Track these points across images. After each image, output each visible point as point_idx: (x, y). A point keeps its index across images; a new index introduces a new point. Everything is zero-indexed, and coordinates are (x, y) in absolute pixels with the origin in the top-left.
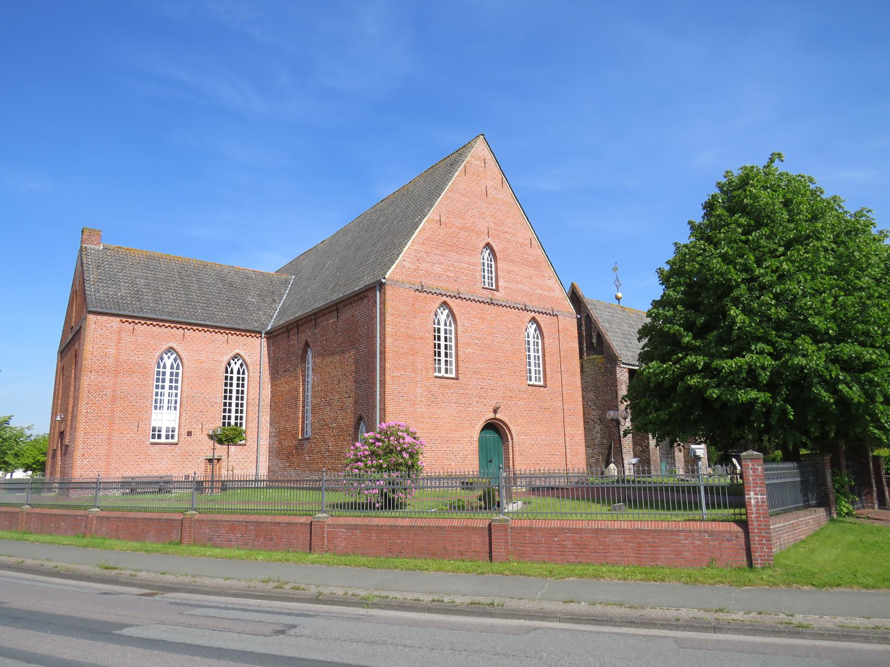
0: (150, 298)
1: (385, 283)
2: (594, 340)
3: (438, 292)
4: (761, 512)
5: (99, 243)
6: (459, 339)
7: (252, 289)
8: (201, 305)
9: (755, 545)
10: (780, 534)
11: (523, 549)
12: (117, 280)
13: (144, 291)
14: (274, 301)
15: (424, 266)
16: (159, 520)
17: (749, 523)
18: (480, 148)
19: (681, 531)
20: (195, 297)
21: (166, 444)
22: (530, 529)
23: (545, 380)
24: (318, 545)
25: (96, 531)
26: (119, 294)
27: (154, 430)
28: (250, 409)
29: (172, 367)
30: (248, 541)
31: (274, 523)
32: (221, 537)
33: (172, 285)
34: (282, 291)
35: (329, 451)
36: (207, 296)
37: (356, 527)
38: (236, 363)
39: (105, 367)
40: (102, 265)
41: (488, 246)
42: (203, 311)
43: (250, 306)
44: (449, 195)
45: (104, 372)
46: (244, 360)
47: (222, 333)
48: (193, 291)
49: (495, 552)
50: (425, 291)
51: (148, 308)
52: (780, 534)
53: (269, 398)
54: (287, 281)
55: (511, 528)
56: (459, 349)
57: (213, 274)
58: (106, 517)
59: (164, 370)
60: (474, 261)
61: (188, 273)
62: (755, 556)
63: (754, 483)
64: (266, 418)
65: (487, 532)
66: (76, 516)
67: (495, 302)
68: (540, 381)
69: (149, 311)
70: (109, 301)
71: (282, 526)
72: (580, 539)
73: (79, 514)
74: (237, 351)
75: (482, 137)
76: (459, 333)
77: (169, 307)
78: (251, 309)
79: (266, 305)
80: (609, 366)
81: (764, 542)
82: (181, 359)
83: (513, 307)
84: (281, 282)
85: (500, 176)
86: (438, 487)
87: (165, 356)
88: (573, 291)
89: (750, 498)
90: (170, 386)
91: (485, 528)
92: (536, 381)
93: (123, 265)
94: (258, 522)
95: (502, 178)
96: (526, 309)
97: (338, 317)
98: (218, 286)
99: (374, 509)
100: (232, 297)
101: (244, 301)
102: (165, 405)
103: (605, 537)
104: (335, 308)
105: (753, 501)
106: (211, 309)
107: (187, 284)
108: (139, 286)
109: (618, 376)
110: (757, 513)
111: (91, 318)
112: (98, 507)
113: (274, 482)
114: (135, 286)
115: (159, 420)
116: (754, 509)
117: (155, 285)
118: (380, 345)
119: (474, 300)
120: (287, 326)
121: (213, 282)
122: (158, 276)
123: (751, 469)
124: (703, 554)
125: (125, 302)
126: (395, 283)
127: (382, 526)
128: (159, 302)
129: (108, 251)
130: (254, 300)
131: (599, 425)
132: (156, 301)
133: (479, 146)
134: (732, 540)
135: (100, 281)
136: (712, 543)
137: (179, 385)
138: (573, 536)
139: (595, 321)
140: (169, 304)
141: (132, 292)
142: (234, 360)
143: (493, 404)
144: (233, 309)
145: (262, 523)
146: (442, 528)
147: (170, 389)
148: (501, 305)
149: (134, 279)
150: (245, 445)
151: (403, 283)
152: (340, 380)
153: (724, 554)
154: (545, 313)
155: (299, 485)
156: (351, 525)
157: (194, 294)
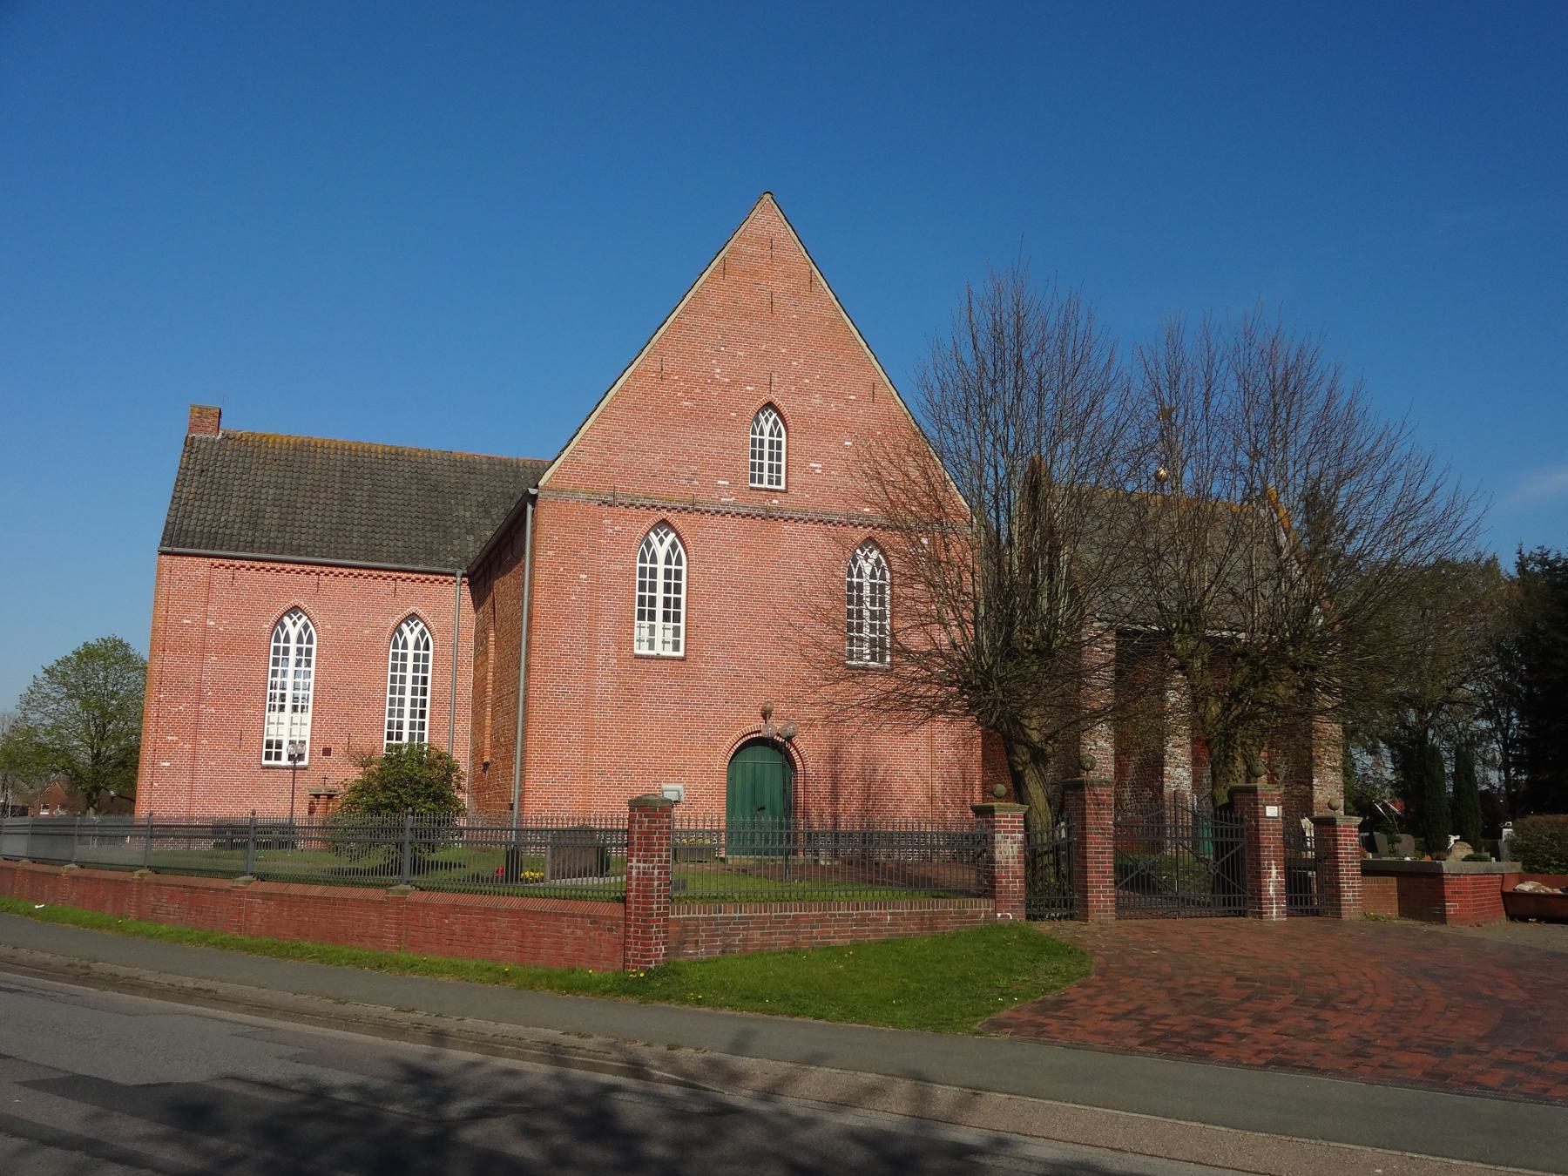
0: (274, 522)
13: (268, 509)
15: (621, 458)
18: (766, 220)
22: (424, 905)
27: (269, 745)
36: (378, 512)
39: (186, 642)
44: (686, 320)
74: (412, 609)
75: (768, 196)
78: (456, 531)
103: (492, 921)
106: (377, 536)
115: (273, 723)
121: (401, 485)
127: (294, 896)
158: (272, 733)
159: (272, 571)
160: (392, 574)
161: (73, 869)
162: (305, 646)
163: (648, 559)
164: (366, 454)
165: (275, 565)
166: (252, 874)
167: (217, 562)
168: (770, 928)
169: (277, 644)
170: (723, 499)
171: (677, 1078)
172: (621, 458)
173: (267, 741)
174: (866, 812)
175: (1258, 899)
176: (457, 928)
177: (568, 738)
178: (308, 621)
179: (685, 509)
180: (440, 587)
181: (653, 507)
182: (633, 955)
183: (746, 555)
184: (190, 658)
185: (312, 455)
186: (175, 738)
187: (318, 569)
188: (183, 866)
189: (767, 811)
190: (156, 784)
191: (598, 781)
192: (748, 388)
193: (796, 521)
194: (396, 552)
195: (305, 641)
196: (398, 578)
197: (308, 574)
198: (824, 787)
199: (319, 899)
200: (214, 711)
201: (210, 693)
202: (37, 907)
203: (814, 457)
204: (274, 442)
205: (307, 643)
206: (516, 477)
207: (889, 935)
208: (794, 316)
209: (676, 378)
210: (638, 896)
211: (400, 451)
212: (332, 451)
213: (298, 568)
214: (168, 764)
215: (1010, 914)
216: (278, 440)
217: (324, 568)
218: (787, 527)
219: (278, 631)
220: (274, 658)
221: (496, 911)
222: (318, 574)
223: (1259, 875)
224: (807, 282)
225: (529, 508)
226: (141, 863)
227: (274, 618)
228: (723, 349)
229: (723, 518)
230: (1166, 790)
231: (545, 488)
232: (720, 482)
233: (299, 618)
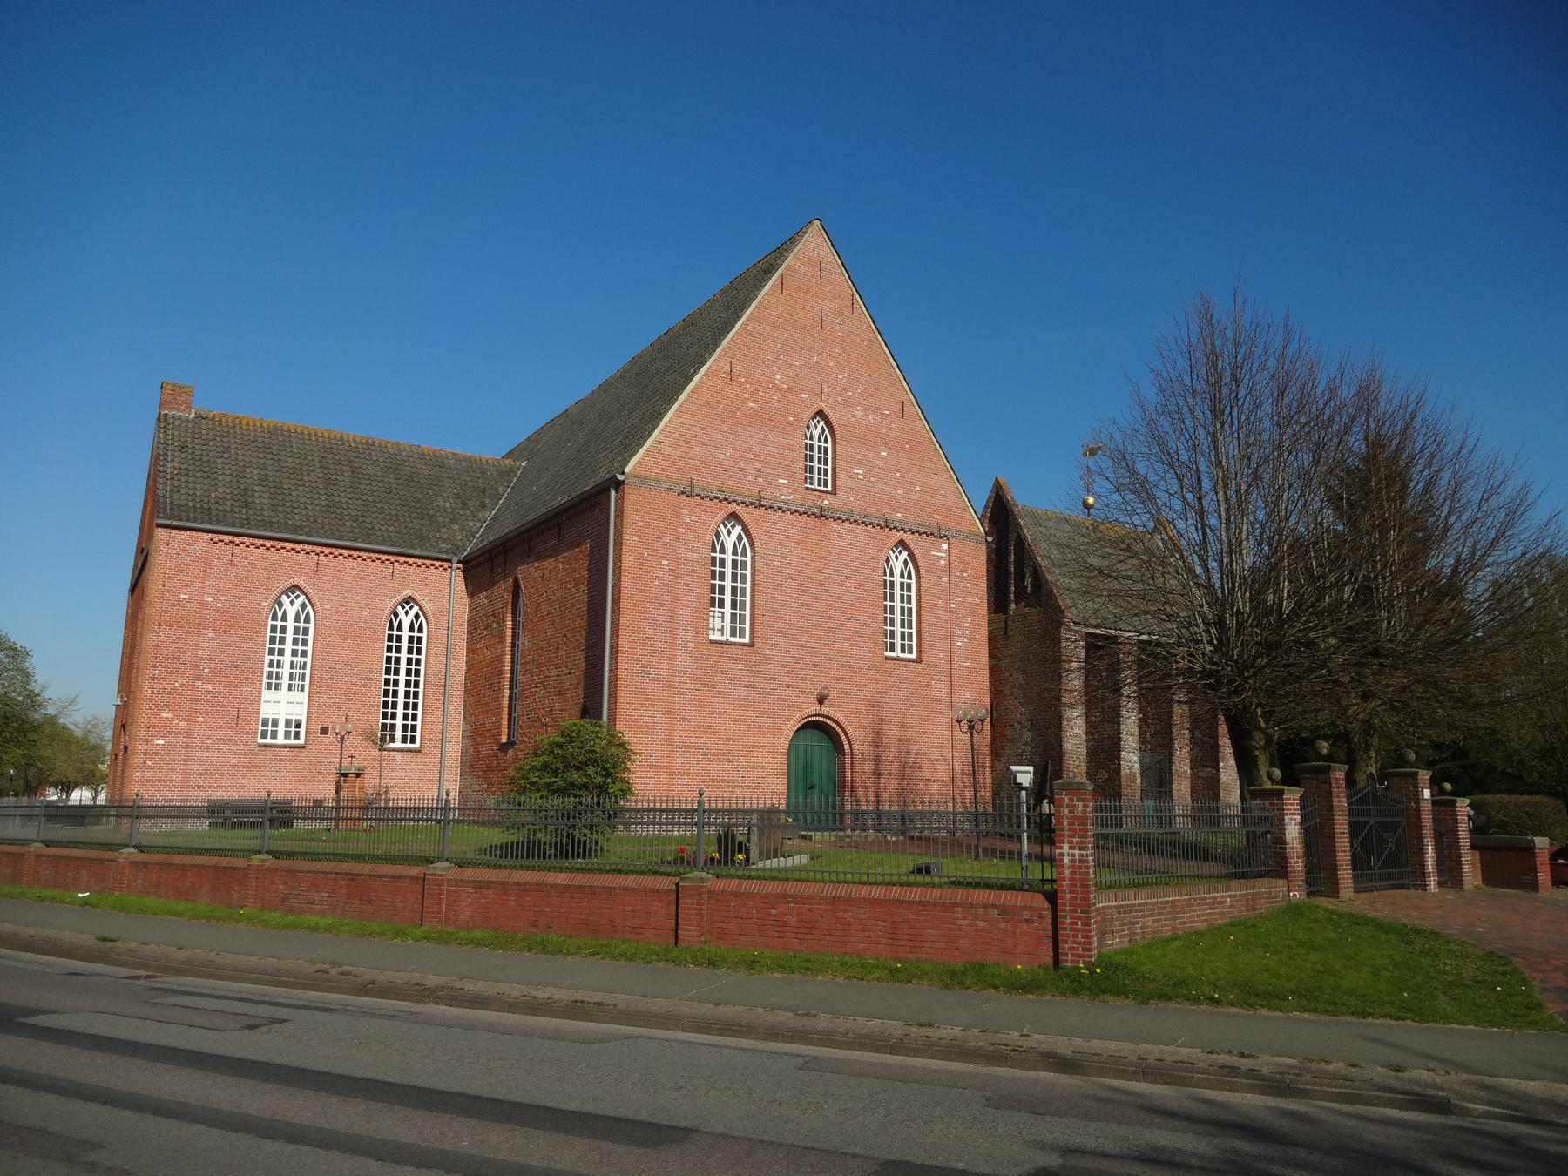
0: (265, 501)
1: (623, 481)
2: (1028, 582)
4: (1078, 877)
5: (189, 408)
6: (758, 579)
7: (448, 485)
8: (353, 513)
9: (1066, 931)
10: (1137, 917)
11: (725, 925)
12: (213, 471)
13: (257, 489)
14: (483, 506)
15: (696, 451)
16: (215, 868)
17: (1059, 894)
18: (814, 244)
19: (957, 905)
20: (344, 500)
22: (737, 895)
23: (919, 651)
25: (129, 886)
26: (213, 495)
27: (265, 723)
29: (297, 619)
30: (336, 904)
33: (306, 479)
34: (500, 489)
36: (364, 497)
37: (488, 884)
38: (407, 613)
40: (190, 446)
41: (820, 414)
42: (355, 525)
43: (438, 514)
44: (750, 327)
48: (342, 489)
49: (683, 929)
50: (698, 495)
51: (259, 518)
52: (1137, 917)
53: (464, 672)
55: (710, 892)
57: (381, 460)
59: (283, 623)
61: (337, 458)
62: (1064, 948)
63: (1070, 830)
64: (457, 707)
65: (673, 899)
67: (829, 514)
68: (911, 652)
69: (260, 524)
70: (194, 506)
72: (808, 913)
74: (409, 592)
75: (817, 222)
77: (297, 517)
79: (468, 512)
81: (1080, 926)
84: (501, 474)
88: (997, 493)
89: (1062, 855)
91: (671, 890)
92: (902, 652)
93: (226, 445)
94: (351, 874)
95: (853, 295)
97: (559, 537)
98: (386, 480)
99: (544, 857)
100: (410, 499)
101: (430, 507)
102: (285, 682)
103: (845, 911)
105: (1066, 860)
106: (368, 520)
107: (333, 477)
108: (249, 481)
110: (1071, 879)
114: (242, 481)
116: (1067, 872)
117: (278, 480)
118: (613, 587)
119: (788, 510)
121: (379, 473)
122: (284, 464)
123: (1068, 806)
124: (988, 943)
125: (221, 508)
126: (642, 480)
127: (525, 884)
128: (280, 509)
129: (203, 422)
130: (447, 505)
131: (1028, 730)
132: (274, 508)
133: (811, 239)
134: (1033, 921)
135: (183, 472)
136: (1002, 925)
137: (309, 648)
138: (799, 908)
139: (1030, 546)
140: (296, 511)
141: (235, 492)
142: (403, 607)
143: (816, 689)
144: (408, 520)
145: (358, 875)
146: (609, 890)
147: (292, 655)
149: (241, 469)
150: (420, 751)
151: (657, 481)
152: (558, 645)
153: (1019, 944)
157: (343, 495)
158: (266, 711)
159: (272, 549)
160: (390, 557)
161: (133, 854)
162: (302, 625)
163: (739, 551)
164: (339, 442)
165: (276, 543)
166: (267, 852)
167: (216, 537)
168: (1159, 914)
169: (274, 623)
170: (783, 497)
171: (1499, 1110)
172: (696, 451)
173: (263, 719)
174: (902, 791)
175: (1421, 872)
176: (792, 920)
177: (653, 717)
178: (306, 601)
179: (752, 504)
180: (436, 572)
181: (725, 499)
182: (1071, 949)
183: (803, 550)
184: (187, 633)
185: (287, 439)
186: (170, 716)
187: (318, 549)
188: (160, 842)
189: (817, 790)
190: (150, 763)
191: (679, 760)
192: (803, 395)
193: (843, 522)
194: (389, 537)
195: (302, 621)
196: (396, 561)
197: (307, 553)
198: (868, 768)
199: (564, 889)
200: (210, 688)
201: (206, 670)
202: (80, 895)
203: (858, 464)
204: (248, 424)
205: (304, 622)
206: (483, 473)
207: (1231, 918)
208: (840, 334)
209: (743, 380)
210: (1074, 886)
211: (370, 441)
212: (306, 437)
213: (298, 547)
214: (162, 742)
215: (1297, 895)
216: (251, 423)
217: (324, 549)
218: (836, 526)
219: (275, 610)
220: (271, 636)
221: (850, 901)
222: (317, 554)
223: (1421, 851)
224: (850, 304)
225: (613, 493)
226: (35, 838)
227: (272, 597)
228: (782, 357)
229: (784, 514)
230: (1123, 772)
231: (629, 476)
232: (781, 481)
233: (297, 597)
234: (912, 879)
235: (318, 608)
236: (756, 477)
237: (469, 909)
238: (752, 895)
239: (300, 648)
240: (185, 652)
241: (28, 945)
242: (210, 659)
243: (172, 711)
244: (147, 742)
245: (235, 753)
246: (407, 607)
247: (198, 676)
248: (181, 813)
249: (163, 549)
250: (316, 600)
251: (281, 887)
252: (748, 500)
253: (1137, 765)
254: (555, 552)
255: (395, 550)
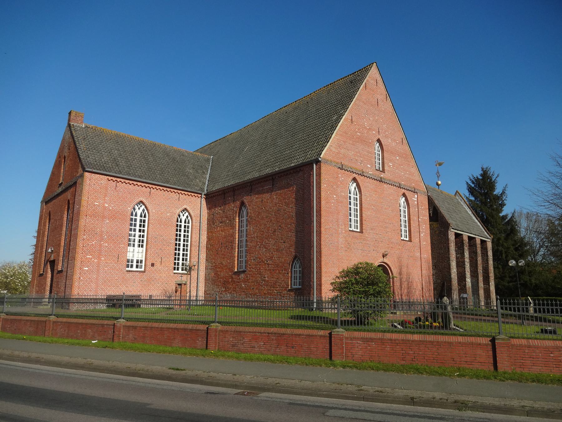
3: (351, 170)
5: (82, 123)
11: (523, 361)
15: (342, 151)
16: (185, 330)
18: (374, 72)
21: (137, 272)
23: (410, 237)
24: (339, 353)
27: (128, 261)
28: (193, 249)
31: (295, 335)
32: (245, 344)
34: (207, 166)
35: (265, 281)
37: (372, 340)
39: (96, 213)
41: (379, 141)
45: (96, 217)
46: (189, 214)
47: (175, 193)
53: (206, 241)
54: (208, 160)
56: (363, 212)
58: (133, 327)
60: (371, 150)
66: (103, 325)
67: (383, 181)
71: (303, 337)
73: (105, 323)
74: (185, 206)
76: (363, 200)
80: (443, 230)
82: (147, 210)
83: (393, 185)
85: (385, 93)
86: (174, 305)
87: (136, 207)
90: (139, 229)
94: (279, 334)
95: (386, 94)
96: (400, 187)
104: (271, 178)
109: (449, 237)
111: (87, 174)
112: (123, 318)
113: (210, 300)
114: (112, 155)
120: (224, 190)
126: (327, 161)
127: (395, 340)
129: (89, 129)
139: (432, 199)
142: (182, 213)
143: (383, 251)
145: (284, 334)
146: (450, 343)
148: (386, 183)
154: (411, 190)
155: (226, 304)
156: (367, 338)
158: (130, 256)
167: (110, 178)
186: (90, 257)
187: (151, 186)
200: (107, 245)
201: (105, 237)
203: (391, 161)
218: (385, 186)
222: (150, 188)
231: (322, 159)
234: (538, 336)
235: (150, 212)
236: (361, 163)
237: (360, 352)
238: (537, 347)
239: (142, 228)
240: (97, 229)
241: (11, 358)
242: (107, 232)
243: (91, 255)
244: (81, 268)
245: (117, 274)
246: (184, 213)
247: (102, 239)
248: (96, 301)
249: (88, 182)
250: (149, 208)
251: (231, 339)
252: (359, 173)
253: (470, 284)
254: (271, 191)
255: (181, 188)
